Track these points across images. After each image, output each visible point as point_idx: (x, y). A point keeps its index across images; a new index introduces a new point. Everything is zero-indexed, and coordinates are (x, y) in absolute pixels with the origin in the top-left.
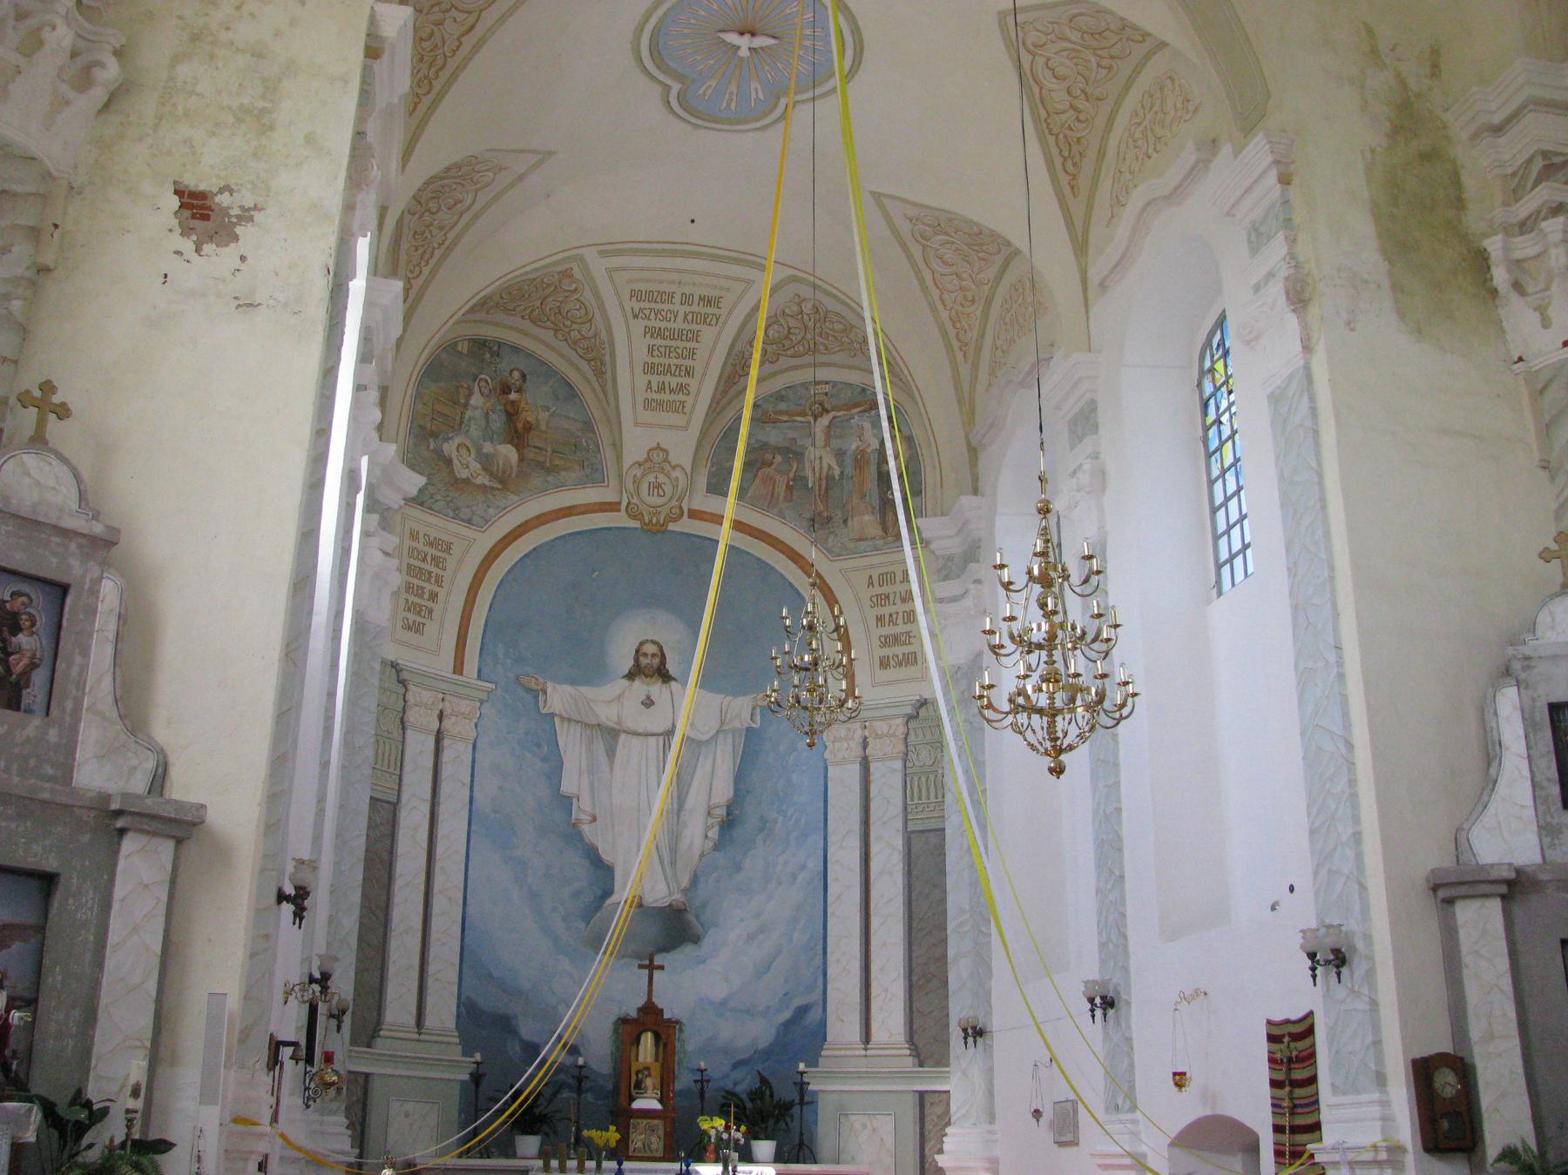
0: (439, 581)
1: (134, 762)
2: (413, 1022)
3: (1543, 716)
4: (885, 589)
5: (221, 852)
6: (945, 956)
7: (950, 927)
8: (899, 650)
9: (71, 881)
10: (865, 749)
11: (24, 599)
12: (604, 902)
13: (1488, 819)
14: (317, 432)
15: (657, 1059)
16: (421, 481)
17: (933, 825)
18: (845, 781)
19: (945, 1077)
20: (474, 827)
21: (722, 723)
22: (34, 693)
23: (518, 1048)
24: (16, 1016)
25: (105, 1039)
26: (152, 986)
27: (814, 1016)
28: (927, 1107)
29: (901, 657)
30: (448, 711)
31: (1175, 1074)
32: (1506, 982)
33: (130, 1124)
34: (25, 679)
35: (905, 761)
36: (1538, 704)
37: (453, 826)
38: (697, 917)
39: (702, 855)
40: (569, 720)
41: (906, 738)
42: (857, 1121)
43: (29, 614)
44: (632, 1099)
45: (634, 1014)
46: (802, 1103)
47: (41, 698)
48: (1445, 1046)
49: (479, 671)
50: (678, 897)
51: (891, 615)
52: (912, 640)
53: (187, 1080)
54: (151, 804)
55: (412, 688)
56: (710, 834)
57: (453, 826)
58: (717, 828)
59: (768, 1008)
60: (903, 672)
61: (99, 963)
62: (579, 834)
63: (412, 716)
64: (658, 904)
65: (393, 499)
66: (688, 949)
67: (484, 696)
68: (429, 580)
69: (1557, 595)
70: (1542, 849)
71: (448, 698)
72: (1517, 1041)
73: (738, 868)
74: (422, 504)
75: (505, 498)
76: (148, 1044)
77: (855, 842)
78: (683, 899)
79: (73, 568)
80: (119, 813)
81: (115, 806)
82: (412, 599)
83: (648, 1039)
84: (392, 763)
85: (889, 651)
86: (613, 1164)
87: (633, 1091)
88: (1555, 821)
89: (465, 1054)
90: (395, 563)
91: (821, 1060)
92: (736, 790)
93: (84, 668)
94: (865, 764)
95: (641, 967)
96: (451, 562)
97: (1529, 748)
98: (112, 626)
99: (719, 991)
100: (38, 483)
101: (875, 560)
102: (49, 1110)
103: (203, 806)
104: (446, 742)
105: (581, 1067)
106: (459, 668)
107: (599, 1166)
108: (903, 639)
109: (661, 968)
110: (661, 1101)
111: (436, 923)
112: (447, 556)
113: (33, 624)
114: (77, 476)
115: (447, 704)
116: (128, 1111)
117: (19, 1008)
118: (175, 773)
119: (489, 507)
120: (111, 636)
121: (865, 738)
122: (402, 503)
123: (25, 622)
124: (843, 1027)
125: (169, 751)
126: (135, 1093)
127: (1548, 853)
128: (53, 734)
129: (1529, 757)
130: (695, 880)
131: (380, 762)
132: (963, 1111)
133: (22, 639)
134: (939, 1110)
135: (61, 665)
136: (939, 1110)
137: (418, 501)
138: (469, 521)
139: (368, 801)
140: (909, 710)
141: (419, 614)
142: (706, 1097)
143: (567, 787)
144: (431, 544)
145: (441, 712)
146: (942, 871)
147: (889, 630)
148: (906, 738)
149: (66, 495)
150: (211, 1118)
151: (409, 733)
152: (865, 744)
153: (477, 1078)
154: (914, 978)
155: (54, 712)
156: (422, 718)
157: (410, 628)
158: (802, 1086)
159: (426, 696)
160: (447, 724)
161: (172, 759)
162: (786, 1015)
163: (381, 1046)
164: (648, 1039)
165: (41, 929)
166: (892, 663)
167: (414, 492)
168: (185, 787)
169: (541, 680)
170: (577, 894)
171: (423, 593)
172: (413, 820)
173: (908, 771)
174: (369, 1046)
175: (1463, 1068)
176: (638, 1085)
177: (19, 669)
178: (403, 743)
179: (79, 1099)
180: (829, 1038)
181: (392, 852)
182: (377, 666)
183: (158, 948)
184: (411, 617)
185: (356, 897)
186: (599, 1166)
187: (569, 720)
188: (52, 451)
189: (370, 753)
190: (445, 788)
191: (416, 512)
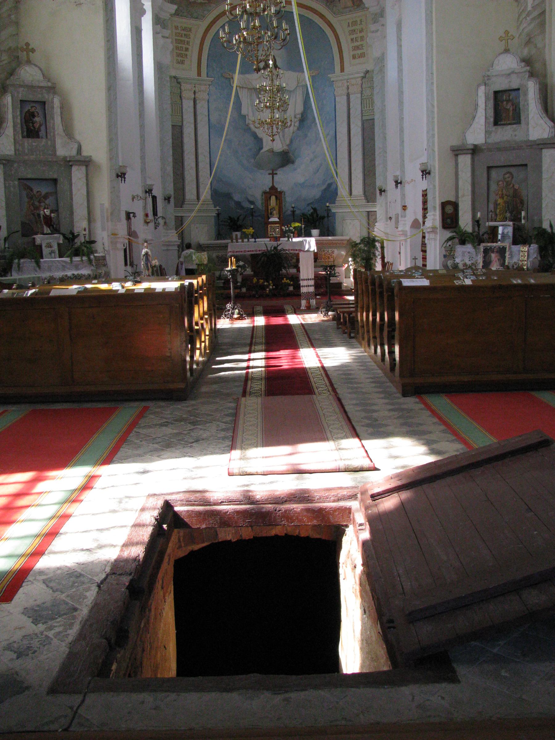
0: (188, 43)
1: (72, 146)
2: (195, 198)
3: (492, 95)
4: (354, 28)
5: (98, 167)
6: (375, 164)
7: (376, 154)
8: (359, 52)
9: (61, 180)
10: (348, 90)
11: (35, 108)
12: (260, 152)
13: (471, 130)
14: (107, 41)
15: (277, 204)
16: (175, 7)
17: (371, 117)
18: (341, 102)
19: (375, 206)
20: (211, 130)
21: (298, 83)
22: (42, 133)
23: (233, 203)
24: (53, 215)
25: (76, 218)
26: (86, 204)
27: (334, 186)
28: (370, 216)
29: (359, 54)
30: (197, 91)
31: (403, 206)
32: (469, 180)
33: (85, 237)
34: (39, 130)
35: (362, 94)
36: (490, 91)
37: (203, 131)
38: (293, 154)
39: (293, 133)
40: (243, 87)
41: (362, 86)
42: (348, 222)
43: (37, 112)
44: (269, 218)
45: (268, 190)
46: (328, 216)
47: (44, 134)
48: (453, 199)
49: (207, 74)
50: (285, 148)
51: (356, 38)
52: (363, 48)
53: (98, 226)
54: (78, 158)
55: (183, 84)
56: (296, 125)
57: (203, 131)
58: (298, 122)
59: (318, 184)
60: (361, 60)
61: (72, 199)
62: (250, 129)
63: (184, 95)
64: (279, 151)
65: (165, 16)
66: (290, 166)
67: (210, 83)
68: (184, 44)
69: (501, 53)
70: (485, 139)
71: (197, 86)
72: (470, 197)
73: (306, 136)
74: (178, 15)
75: (210, 6)
76: (87, 218)
77: (345, 125)
78: (287, 148)
79: (46, 97)
80: (70, 161)
81: (68, 159)
82: (178, 52)
83: (273, 198)
84: (179, 112)
85: (355, 52)
86: (253, 240)
87: (269, 216)
88: (490, 130)
89: (215, 207)
90: (169, 40)
91: (336, 202)
92: (304, 107)
93: (54, 124)
94: (348, 95)
95: (269, 174)
96: (192, 36)
97: (486, 106)
98: (59, 110)
99: (301, 180)
100: (31, 74)
101: (349, 16)
102: (64, 235)
103: (91, 156)
104: (198, 102)
105: (252, 209)
106: (199, 74)
107: (248, 240)
108: (360, 47)
109: (276, 174)
110: (279, 218)
111: (201, 165)
112: (190, 33)
113: (38, 114)
114: (41, 69)
115: (197, 88)
116: (84, 234)
117: (53, 213)
118: (83, 148)
119: (204, 11)
120: (59, 114)
121: (348, 86)
122: (170, 16)
123: (36, 114)
124: (343, 191)
125: (80, 142)
126: (85, 230)
127: (487, 140)
128: (49, 143)
129: (486, 109)
130: (291, 141)
131: (174, 112)
132: (381, 217)
133: (37, 119)
134: (374, 217)
135: (48, 124)
136: (374, 217)
137: (177, 13)
138: (197, 18)
139: (171, 126)
140: (362, 75)
141: (182, 57)
142: (294, 217)
143: (244, 112)
144: (184, 30)
145: (195, 91)
146: (373, 133)
147: (356, 44)
148: (362, 86)
149: (39, 77)
150: (105, 235)
151: (184, 100)
152: (348, 88)
153: (218, 215)
154: (366, 173)
155: (49, 137)
156: (188, 94)
157: (179, 63)
158: (328, 210)
159: (188, 87)
160: (197, 95)
161: (82, 144)
162: (324, 187)
163: (185, 207)
164: (273, 198)
165: (56, 193)
166: (357, 57)
167: (174, 12)
168: (86, 153)
169: (231, 74)
170: (250, 149)
171: (183, 49)
172: (188, 131)
173: (363, 98)
174: (181, 207)
175: (455, 205)
176: (271, 213)
177: (37, 127)
178: (182, 104)
179: (72, 233)
180: (339, 193)
181: (182, 142)
182: (168, 79)
183: (85, 194)
184: (180, 59)
185: (171, 159)
186: (248, 240)
187: (243, 87)
188: (34, 65)
189: (170, 110)
190: (199, 118)
191: (175, 19)
